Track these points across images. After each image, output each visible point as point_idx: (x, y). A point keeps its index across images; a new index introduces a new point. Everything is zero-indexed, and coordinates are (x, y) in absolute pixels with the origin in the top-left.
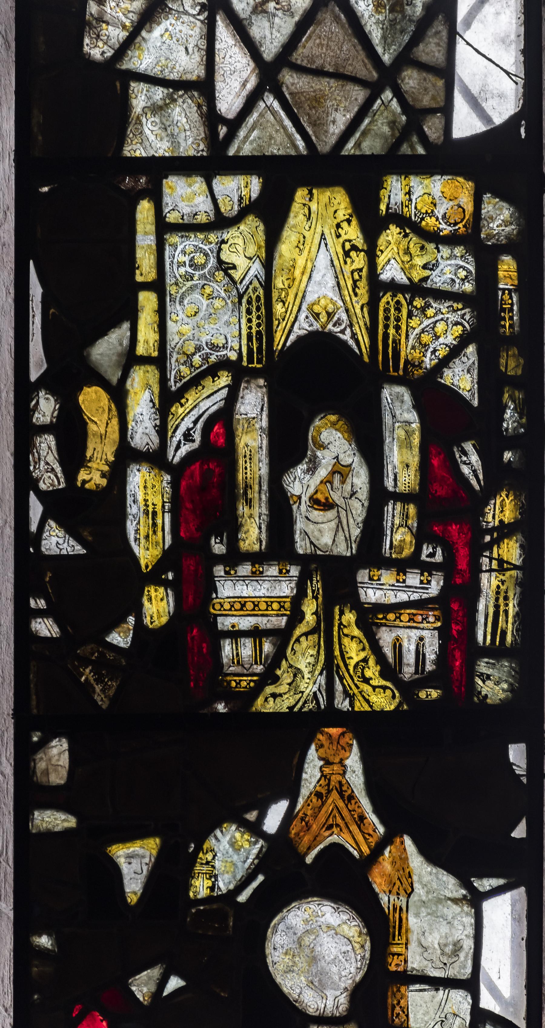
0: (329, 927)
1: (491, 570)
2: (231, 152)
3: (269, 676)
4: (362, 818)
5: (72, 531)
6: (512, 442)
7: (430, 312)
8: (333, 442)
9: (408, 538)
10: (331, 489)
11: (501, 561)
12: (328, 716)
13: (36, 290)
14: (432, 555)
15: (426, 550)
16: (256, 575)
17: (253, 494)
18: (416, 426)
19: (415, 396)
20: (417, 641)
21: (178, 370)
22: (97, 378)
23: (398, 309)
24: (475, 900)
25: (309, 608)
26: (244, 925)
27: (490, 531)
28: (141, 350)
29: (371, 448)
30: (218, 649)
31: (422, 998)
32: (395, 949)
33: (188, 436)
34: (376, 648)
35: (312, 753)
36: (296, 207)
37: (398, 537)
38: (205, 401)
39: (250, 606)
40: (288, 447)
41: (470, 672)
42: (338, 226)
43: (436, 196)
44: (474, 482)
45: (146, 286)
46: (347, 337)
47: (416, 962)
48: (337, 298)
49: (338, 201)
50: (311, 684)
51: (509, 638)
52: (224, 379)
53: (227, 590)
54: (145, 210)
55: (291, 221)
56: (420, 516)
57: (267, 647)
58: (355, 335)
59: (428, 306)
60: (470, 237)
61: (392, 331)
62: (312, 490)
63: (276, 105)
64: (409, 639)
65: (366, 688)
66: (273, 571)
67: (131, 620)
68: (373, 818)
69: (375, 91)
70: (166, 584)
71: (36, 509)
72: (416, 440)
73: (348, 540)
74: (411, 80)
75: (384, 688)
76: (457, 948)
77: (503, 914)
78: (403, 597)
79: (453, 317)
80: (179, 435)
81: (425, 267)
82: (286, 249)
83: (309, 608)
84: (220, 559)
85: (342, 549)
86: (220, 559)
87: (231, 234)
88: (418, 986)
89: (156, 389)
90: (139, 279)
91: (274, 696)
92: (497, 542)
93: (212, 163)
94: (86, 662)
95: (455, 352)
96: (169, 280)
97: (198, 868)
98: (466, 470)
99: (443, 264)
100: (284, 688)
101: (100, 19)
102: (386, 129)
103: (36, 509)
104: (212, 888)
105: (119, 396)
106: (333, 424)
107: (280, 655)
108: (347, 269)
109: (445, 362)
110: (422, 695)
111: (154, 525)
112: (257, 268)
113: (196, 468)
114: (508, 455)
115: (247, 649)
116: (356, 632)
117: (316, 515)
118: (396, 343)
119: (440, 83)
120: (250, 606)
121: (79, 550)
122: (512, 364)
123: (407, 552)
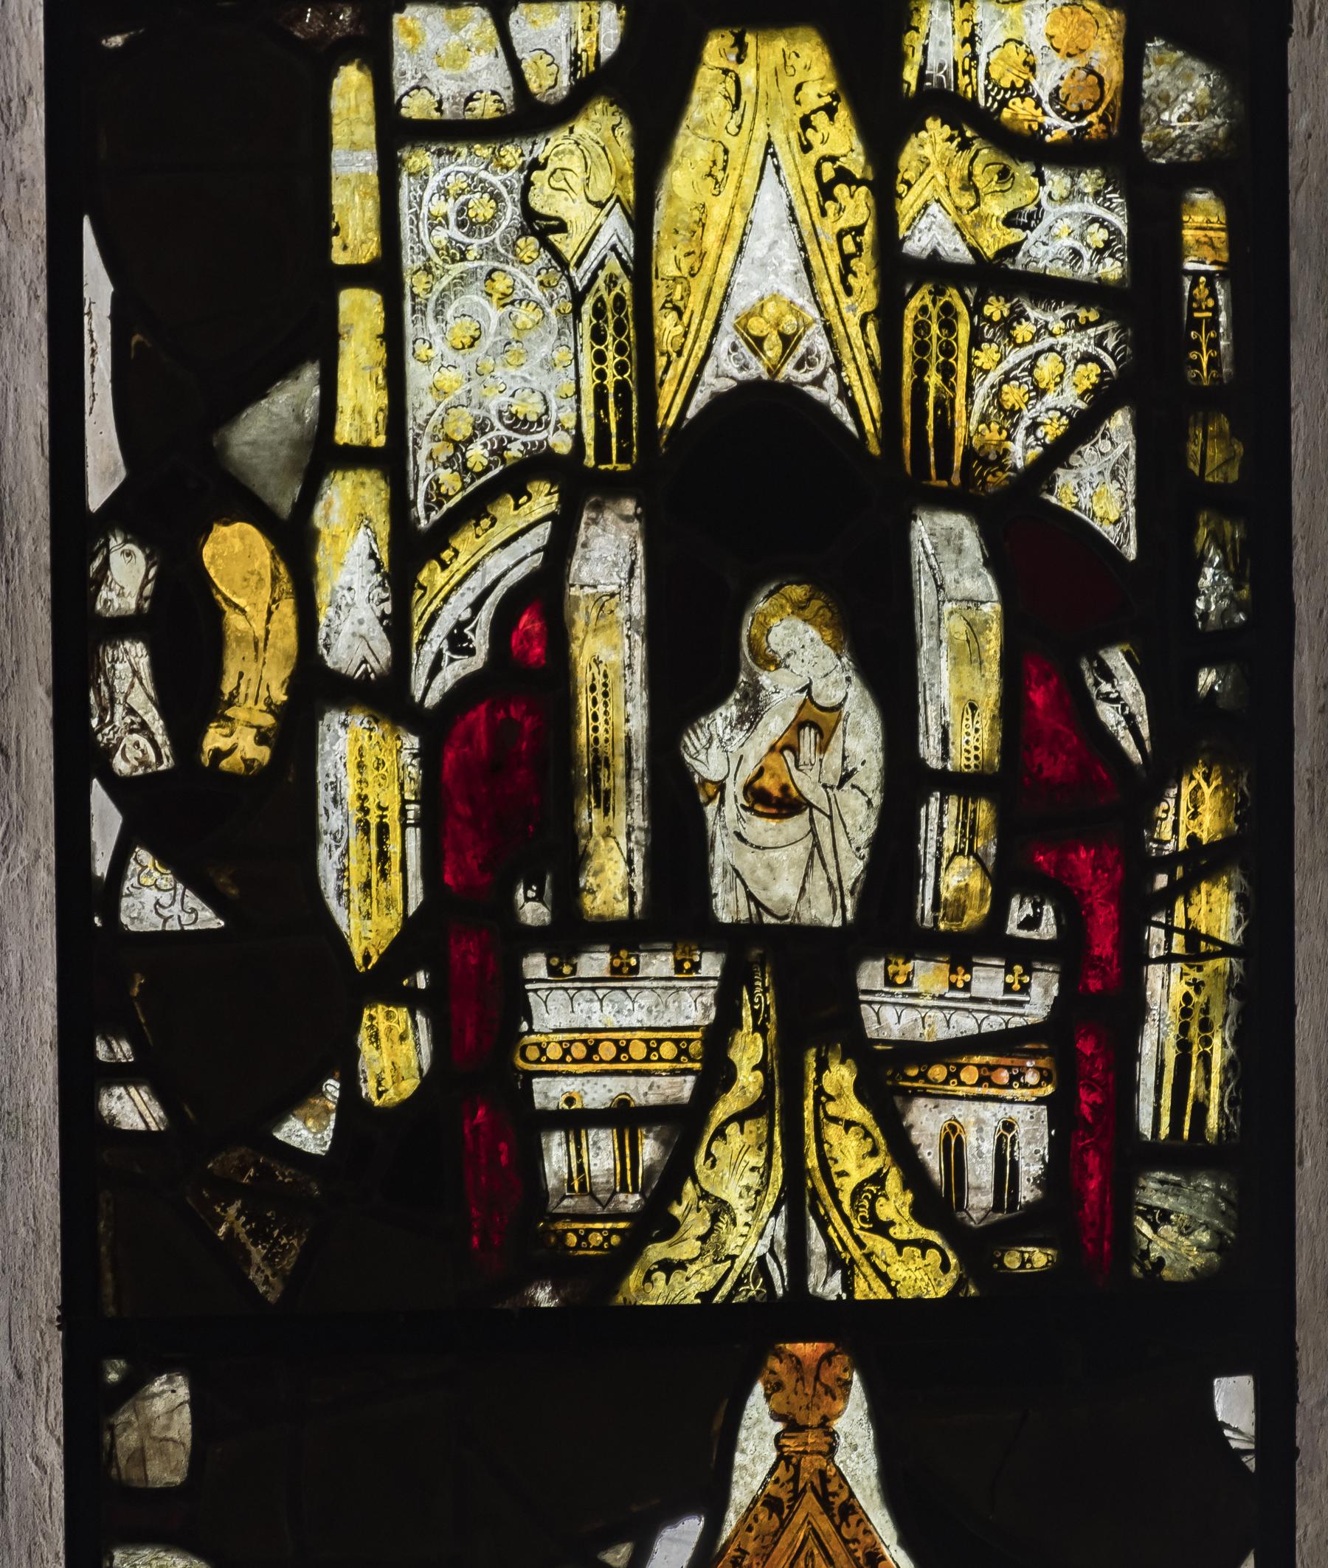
1: (1169, 959)
3: (656, 1221)
5: (191, 874)
6: (1215, 645)
7: (1023, 331)
8: (798, 651)
9: (976, 882)
10: (797, 774)
11: (1193, 936)
13: (98, 289)
15: (1019, 910)
16: (622, 974)
17: (614, 780)
18: (992, 609)
20: (996, 1130)
21: (431, 472)
23: (948, 325)
25: (747, 1052)
28: (345, 433)
29: (887, 663)
30: (537, 1156)
33: (458, 642)
35: (757, 1404)
37: (952, 880)
38: (496, 554)
39: (607, 1051)
40: (695, 663)
41: (1123, 1206)
44: (1128, 744)
45: (357, 276)
46: (827, 394)
48: (803, 300)
50: (752, 1237)
51: (1213, 1120)
52: (542, 500)
53: (554, 1012)
54: (350, 90)
55: (695, 112)
57: (649, 1150)
58: (849, 391)
59: (1018, 315)
60: (1112, 147)
61: (933, 379)
62: (749, 769)
64: (979, 1124)
65: (877, 1244)
66: (660, 964)
67: (332, 1087)
70: (412, 1000)
71: (106, 820)
72: (992, 644)
75: (924, 1245)
78: (965, 1024)
79: (1079, 343)
82: (682, 181)
83: (747, 1052)
85: (822, 911)
89: (383, 529)
90: (340, 257)
91: (668, 1267)
92: (1184, 889)
94: (227, 1190)
95: (1083, 427)
96: (410, 260)
98: (1109, 715)
99: (1051, 211)
100: (688, 1248)
103: (106, 820)
105: (295, 545)
106: (799, 608)
107: (678, 1169)
108: (828, 229)
109: (1058, 454)
110: (1012, 1261)
111: (383, 857)
112: (616, 228)
115: (601, 1155)
116: (858, 1112)
117: (760, 828)
118: (945, 406)
120: (607, 1051)
121: (208, 919)
122: (1216, 454)
123: (975, 914)
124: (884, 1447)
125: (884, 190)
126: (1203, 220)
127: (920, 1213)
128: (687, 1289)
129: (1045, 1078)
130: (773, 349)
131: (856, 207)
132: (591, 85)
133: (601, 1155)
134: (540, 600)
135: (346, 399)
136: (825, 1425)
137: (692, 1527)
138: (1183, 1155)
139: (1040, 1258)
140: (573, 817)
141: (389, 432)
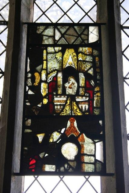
0: (71, 147)
1: (96, 97)
2: (58, 44)
3: (62, 111)
4: (77, 131)
5: (32, 91)
6: (98, 80)
7: (86, 64)
8: (72, 80)
9: (83, 92)
10: (71, 86)
11: (97, 95)
12: (72, 116)
13: (29, 60)
14: (87, 95)
15: (86, 94)
16: (60, 97)
17: (60, 86)
18: (84, 78)
19: (84, 74)
20: (85, 106)
21: (49, 70)
22: (37, 71)
23: (81, 63)
24: (95, 143)
25: (68, 102)
26: (58, 146)
27: (96, 92)
28: (44, 68)
29: (78, 81)
30: (54, 107)
31: (4, 11)
32: (82, 150)
33: (50, 79)
34: (78, 107)
35: (69, 121)
36: (66, 51)
37: (82, 92)
38: (54, 74)
39: (59, 101)
40: (65, 80)
41: (93, 110)
42: (73, 53)
43: (86, 50)
44: (93, 85)
45: (45, 60)
46: (74, 67)
47: (85, 152)
48: (72, 62)
49: (73, 50)
50: (69, 112)
51: (99, 106)
52: (56, 72)
53: (56, 99)
54: (45, 51)
55: (66, 52)
56: (85, 90)
57: (62, 107)
58: (75, 66)
59: (86, 63)
60: (91, 55)
61: (80, 66)
62: (69, 86)
63: (64, 39)
64: (84, 106)
65: (77, 112)
66: (63, 96)
67: (41, 103)
68: (78, 131)
69: (78, 37)
70: (47, 98)
71: (27, 88)
72: (84, 80)
73: (74, 92)
74: (83, 36)
75: (80, 113)
76: (92, 150)
77: (99, 145)
78: (83, 100)
79: (89, 64)
80: (49, 79)
81: (85, 58)
82: (65, 56)
83: (68, 102)
84: (55, 95)
85: (73, 94)
86: (55, 95)
87: (57, 54)
88: (23, 45)
89: (46, 73)
90: (44, 59)
91: (63, 113)
92: (97, 93)
93: (55, 45)
94: (34, 108)
95: (90, 69)
96: (48, 59)
97: (51, 138)
98: (92, 84)
99: (88, 58)
100: (64, 112)
101: (39, 29)
102: (79, 42)
103: (27, 88)
104: (53, 141)
105: (40, 74)
106: (72, 78)
107: (64, 108)
108: (74, 59)
109: (88, 70)
110: (86, 114)
111: (45, 90)
112: (61, 58)
113: (51, 83)
114: (98, 82)
115: (59, 107)
116: (75, 105)
117: (69, 89)
118: (81, 68)
119: (87, 37)
120: (59, 101)
121: (34, 93)
122: (98, 70)
123: (83, 94)
124: (77, 124)
125: (77, 57)
126: (97, 59)
127: (79, 111)
128: (65, 114)
129: (88, 103)
130: (70, 64)
131: (76, 57)
132: (59, 51)
133: (59, 107)
134: (56, 77)
135: (44, 66)
136: (73, 123)
137: (64, 129)
138: (96, 108)
139: (88, 114)
140: (57, 88)
141: (60, 47)
